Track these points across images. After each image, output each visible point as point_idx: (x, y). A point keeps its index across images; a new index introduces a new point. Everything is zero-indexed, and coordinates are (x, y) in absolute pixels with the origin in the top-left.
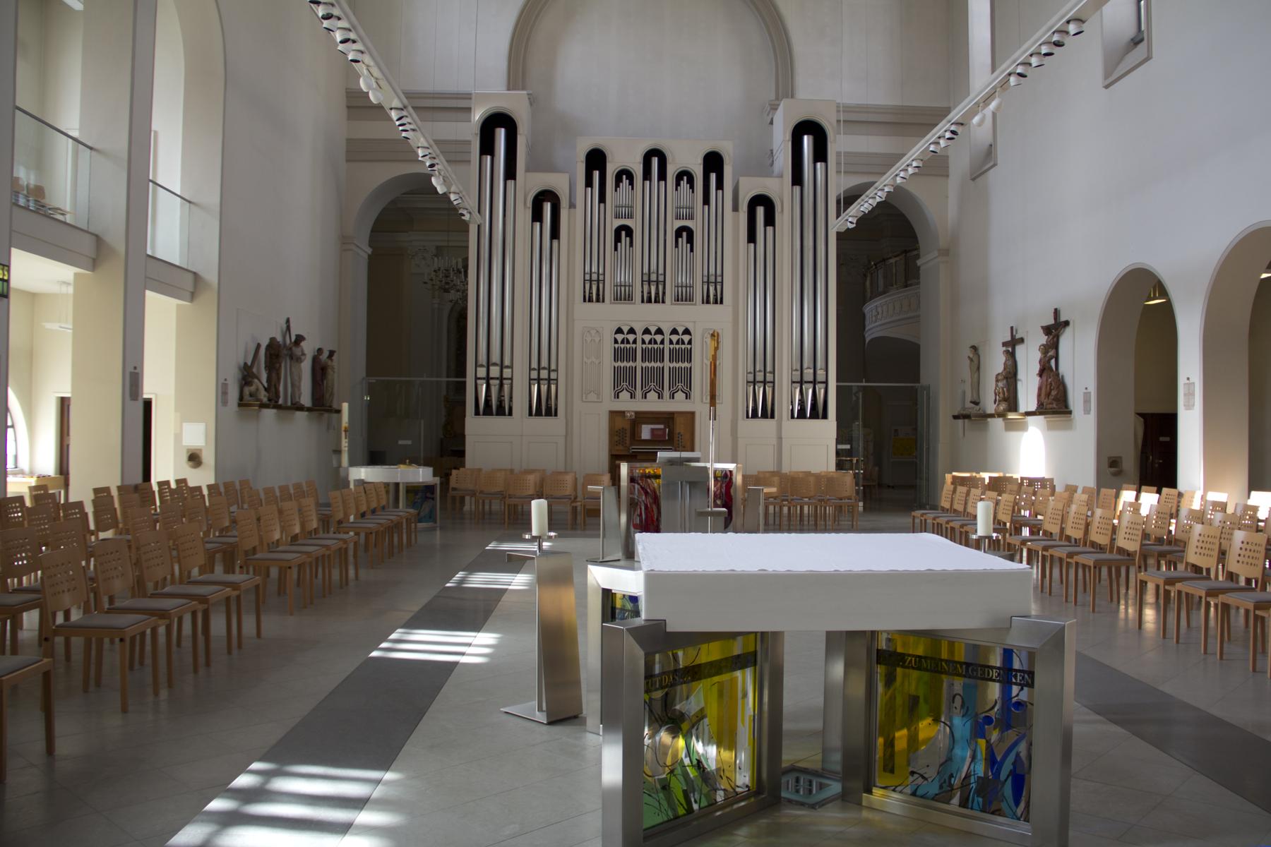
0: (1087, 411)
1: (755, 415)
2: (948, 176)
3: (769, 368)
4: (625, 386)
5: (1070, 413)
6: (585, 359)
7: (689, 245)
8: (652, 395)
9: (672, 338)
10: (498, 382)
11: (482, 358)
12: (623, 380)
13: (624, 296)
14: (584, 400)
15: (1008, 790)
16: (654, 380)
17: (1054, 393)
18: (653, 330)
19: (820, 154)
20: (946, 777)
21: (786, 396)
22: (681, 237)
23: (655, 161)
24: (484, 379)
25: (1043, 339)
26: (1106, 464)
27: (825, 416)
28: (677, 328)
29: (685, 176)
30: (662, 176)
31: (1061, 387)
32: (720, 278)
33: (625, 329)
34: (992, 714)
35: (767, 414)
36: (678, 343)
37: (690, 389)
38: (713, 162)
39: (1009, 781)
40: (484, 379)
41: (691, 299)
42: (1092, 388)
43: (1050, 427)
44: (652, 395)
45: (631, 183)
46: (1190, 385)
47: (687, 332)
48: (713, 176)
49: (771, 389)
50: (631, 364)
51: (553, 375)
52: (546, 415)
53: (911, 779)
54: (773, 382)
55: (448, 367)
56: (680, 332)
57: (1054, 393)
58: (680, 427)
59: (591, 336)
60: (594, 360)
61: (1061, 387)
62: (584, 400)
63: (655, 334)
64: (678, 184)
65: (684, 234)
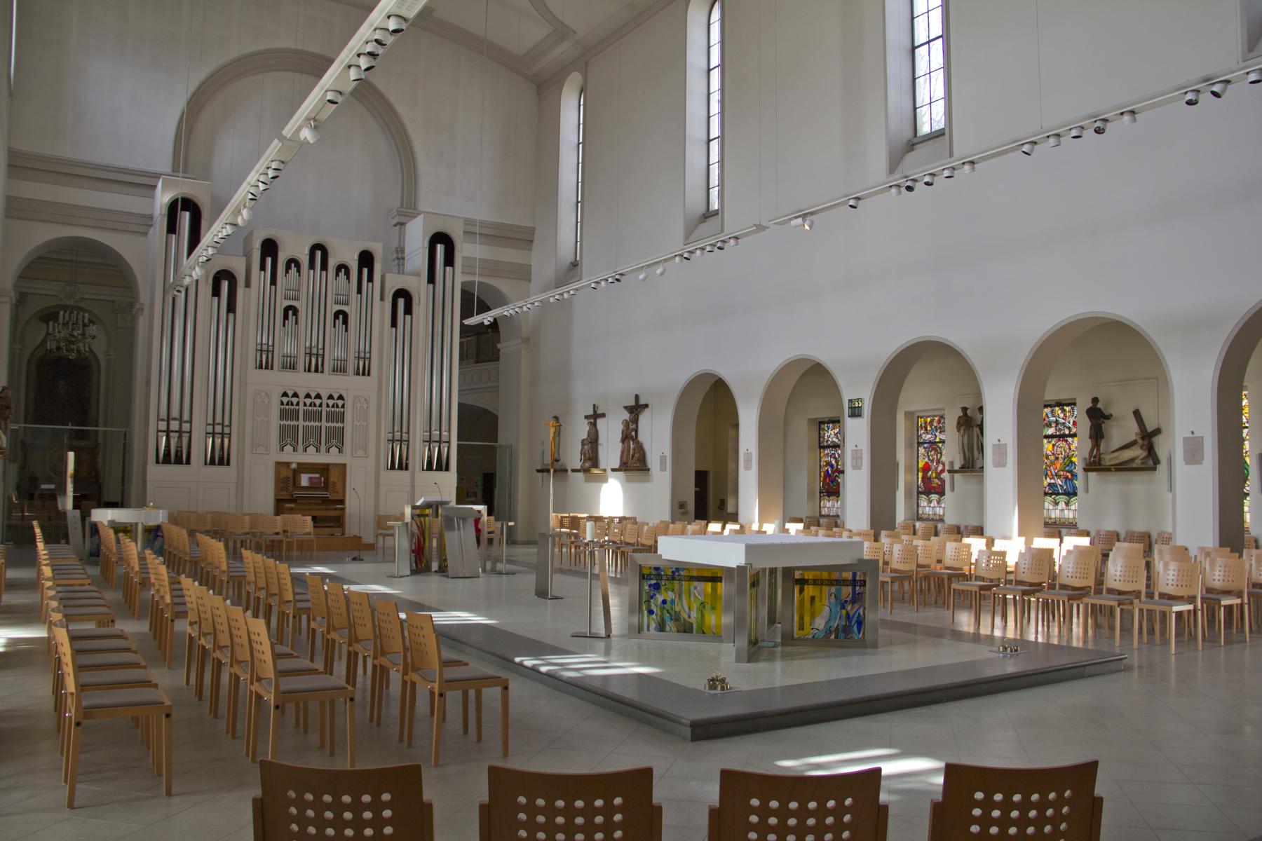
0: (663, 469)
1: (393, 467)
2: (530, 281)
3: (405, 429)
4: (312, 442)
5: (649, 470)
6: (355, 422)
7: (344, 326)
8: (312, 449)
9: (283, 400)
10: (177, 434)
11: (164, 414)
12: (286, 437)
13: (291, 366)
14: (254, 452)
15: (855, 628)
16: (313, 437)
17: (636, 456)
18: (336, 396)
19: (449, 261)
20: (828, 628)
21: (419, 452)
22: (338, 318)
23: (319, 254)
24: (164, 431)
25: (626, 416)
26: (677, 506)
27: (447, 469)
28: (333, 394)
29: (342, 268)
30: (324, 266)
31: (642, 452)
32: (322, 351)
33: (290, 394)
34: (848, 599)
35: (402, 467)
36: (310, 405)
37: (343, 445)
38: (366, 259)
39: (856, 625)
40: (164, 431)
41: (345, 371)
42: (668, 453)
43: (628, 480)
44: (312, 449)
45: (299, 271)
46: (748, 456)
47: (341, 397)
48: (365, 271)
49: (406, 447)
50: (294, 423)
51: (227, 430)
52: (175, 463)
53: (812, 631)
54: (408, 441)
55: (26, 412)
56: (313, 397)
57: (636, 456)
58: (334, 477)
59: (360, 402)
60: (362, 423)
61: (642, 452)
62: (254, 452)
63: (315, 398)
64: (337, 275)
65: (341, 317)
